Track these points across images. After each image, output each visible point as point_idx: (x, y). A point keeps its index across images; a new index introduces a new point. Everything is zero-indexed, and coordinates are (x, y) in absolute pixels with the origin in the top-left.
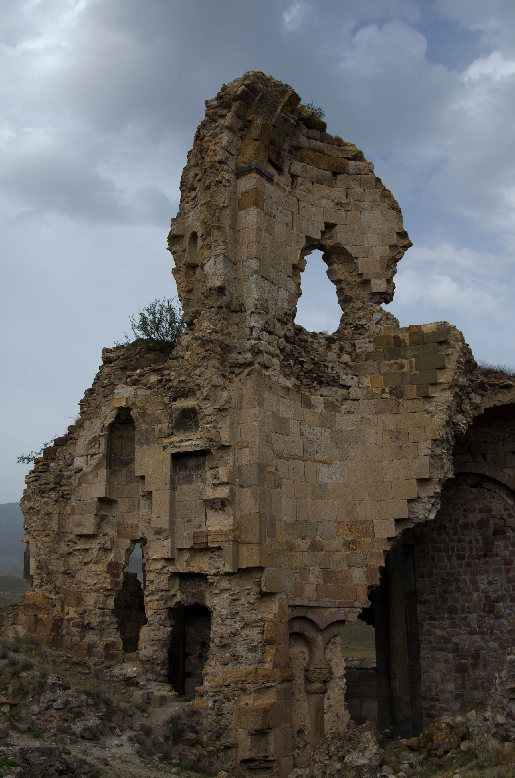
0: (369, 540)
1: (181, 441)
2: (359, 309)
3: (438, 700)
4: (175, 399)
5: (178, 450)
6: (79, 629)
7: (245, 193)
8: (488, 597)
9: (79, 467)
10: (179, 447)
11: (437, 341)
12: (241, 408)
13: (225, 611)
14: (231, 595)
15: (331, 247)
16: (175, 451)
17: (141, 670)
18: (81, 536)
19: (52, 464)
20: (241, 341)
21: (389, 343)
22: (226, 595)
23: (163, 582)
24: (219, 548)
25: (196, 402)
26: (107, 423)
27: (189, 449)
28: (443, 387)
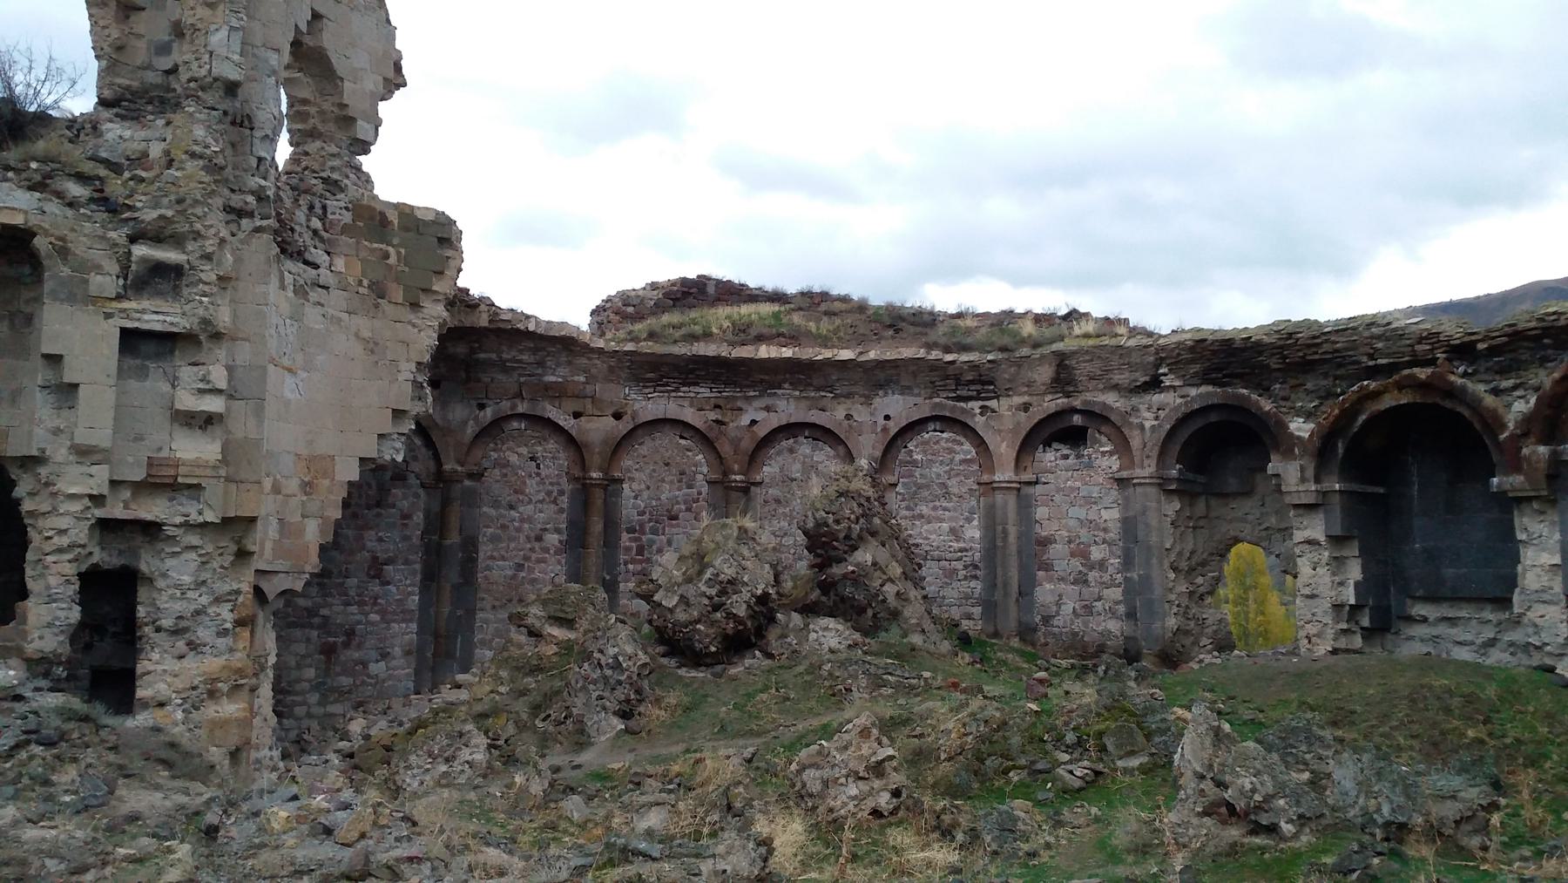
0: (326, 482)
1: (143, 311)
2: (333, 155)
3: (289, 693)
4: (133, 239)
5: (136, 325)
10: (139, 320)
11: (439, 235)
13: (187, 579)
14: (200, 555)
15: (310, 48)
16: (129, 325)
17: (23, 674)
20: (237, 173)
22: (193, 555)
23: (80, 533)
24: (198, 487)
27: (158, 327)
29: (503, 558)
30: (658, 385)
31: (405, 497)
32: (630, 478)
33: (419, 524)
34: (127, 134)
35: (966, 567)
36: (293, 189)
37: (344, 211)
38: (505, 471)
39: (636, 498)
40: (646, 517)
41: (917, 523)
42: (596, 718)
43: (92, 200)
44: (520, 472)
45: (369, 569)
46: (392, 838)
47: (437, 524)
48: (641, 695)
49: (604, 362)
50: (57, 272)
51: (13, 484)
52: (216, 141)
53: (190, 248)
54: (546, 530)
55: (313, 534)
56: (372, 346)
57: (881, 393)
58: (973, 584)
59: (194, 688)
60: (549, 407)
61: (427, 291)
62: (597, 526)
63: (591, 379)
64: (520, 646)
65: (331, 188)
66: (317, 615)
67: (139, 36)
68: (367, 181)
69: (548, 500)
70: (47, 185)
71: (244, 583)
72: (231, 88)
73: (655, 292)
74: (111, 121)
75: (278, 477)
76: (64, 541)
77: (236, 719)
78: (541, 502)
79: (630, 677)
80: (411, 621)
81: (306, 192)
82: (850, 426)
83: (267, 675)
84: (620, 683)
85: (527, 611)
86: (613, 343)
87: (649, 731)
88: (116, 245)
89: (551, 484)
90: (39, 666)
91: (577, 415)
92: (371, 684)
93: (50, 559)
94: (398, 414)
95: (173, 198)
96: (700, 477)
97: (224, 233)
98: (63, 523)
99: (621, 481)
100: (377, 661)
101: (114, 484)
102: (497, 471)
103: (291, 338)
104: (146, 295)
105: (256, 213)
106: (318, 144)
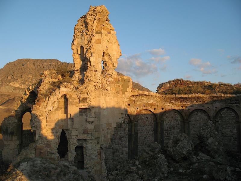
0: (111, 128)
3: (107, 160)
8: (120, 137)
35: (234, 138)
39: (166, 124)
40: (169, 128)
41: (223, 129)
57: (215, 103)
58: (235, 142)
62: (159, 130)
63: (157, 102)
71: (99, 146)
78: (148, 126)
80: (127, 148)
82: (209, 110)
90: (70, 162)
91: (155, 109)
96: (179, 120)
102: (140, 120)
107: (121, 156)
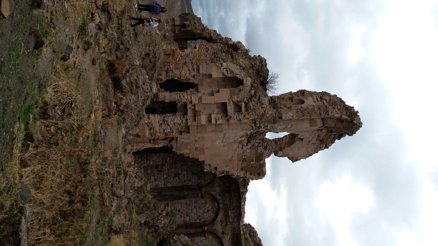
0: (198, 153)
1: (231, 106)
2: (272, 147)
3: (147, 159)
4: (245, 103)
5: (228, 105)
6: (166, 70)
7: (316, 122)
9: (223, 65)
10: (229, 105)
12: (241, 124)
13: (175, 121)
14: (181, 123)
15: (295, 139)
16: (228, 104)
18: (199, 67)
19: (224, 54)
21: (260, 157)
22: (180, 122)
23: (184, 100)
25: (243, 112)
26: (238, 76)
27: (228, 109)
28: (245, 174)
29: (181, 207)
30: (233, 244)
31: (195, 179)
32: (206, 239)
33: (189, 184)
34: (266, 101)
36: (263, 139)
37: (260, 151)
38: (204, 204)
39: (201, 241)
42: (144, 216)
43: (251, 95)
44: (204, 207)
45: (177, 173)
46: (142, 95)
47: (189, 188)
48: (151, 227)
49: (236, 226)
50: (236, 90)
51: (193, 88)
52: (269, 116)
53: (246, 113)
54: (190, 217)
55: (186, 152)
56: (231, 160)
59: (152, 125)
60: (222, 213)
61: (246, 172)
62: (192, 231)
64: (160, 206)
65: (265, 148)
66: (165, 163)
67: (286, 102)
68: (269, 156)
69: (198, 216)
70: (252, 87)
71: (175, 134)
72: (281, 118)
73: (258, 241)
74: (268, 99)
75: (198, 141)
76: (182, 97)
77: (145, 134)
78: (197, 214)
79: (155, 223)
80: (164, 185)
81: (263, 142)
83: (153, 145)
84: (154, 221)
85: (169, 207)
86: (242, 228)
87: (141, 229)
88: (243, 100)
89: (202, 216)
90: (156, 96)
91: (221, 221)
92: (148, 177)
93: (178, 95)
94: (216, 168)
95: (255, 108)
97: (250, 119)
98: (186, 97)
99: (205, 236)
100: (154, 178)
101: (194, 105)
102: (203, 202)
103: (230, 141)
104: (234, 106)
105: (256, 127)
106: (274, 144)
107: (153, 178)
